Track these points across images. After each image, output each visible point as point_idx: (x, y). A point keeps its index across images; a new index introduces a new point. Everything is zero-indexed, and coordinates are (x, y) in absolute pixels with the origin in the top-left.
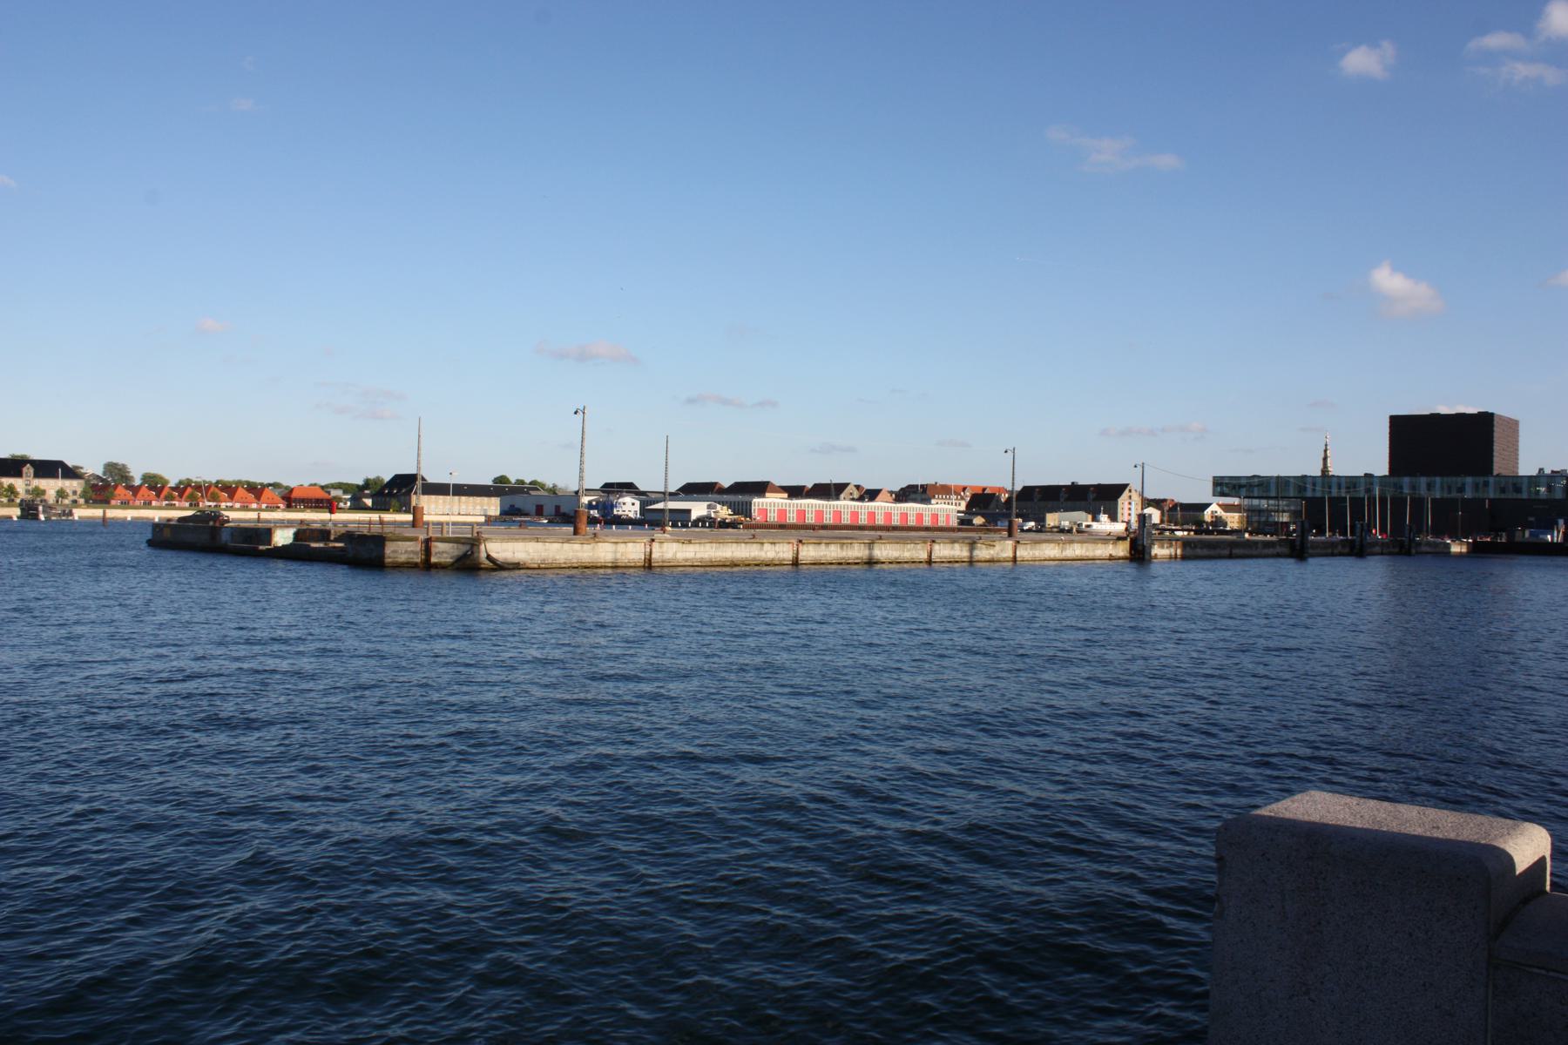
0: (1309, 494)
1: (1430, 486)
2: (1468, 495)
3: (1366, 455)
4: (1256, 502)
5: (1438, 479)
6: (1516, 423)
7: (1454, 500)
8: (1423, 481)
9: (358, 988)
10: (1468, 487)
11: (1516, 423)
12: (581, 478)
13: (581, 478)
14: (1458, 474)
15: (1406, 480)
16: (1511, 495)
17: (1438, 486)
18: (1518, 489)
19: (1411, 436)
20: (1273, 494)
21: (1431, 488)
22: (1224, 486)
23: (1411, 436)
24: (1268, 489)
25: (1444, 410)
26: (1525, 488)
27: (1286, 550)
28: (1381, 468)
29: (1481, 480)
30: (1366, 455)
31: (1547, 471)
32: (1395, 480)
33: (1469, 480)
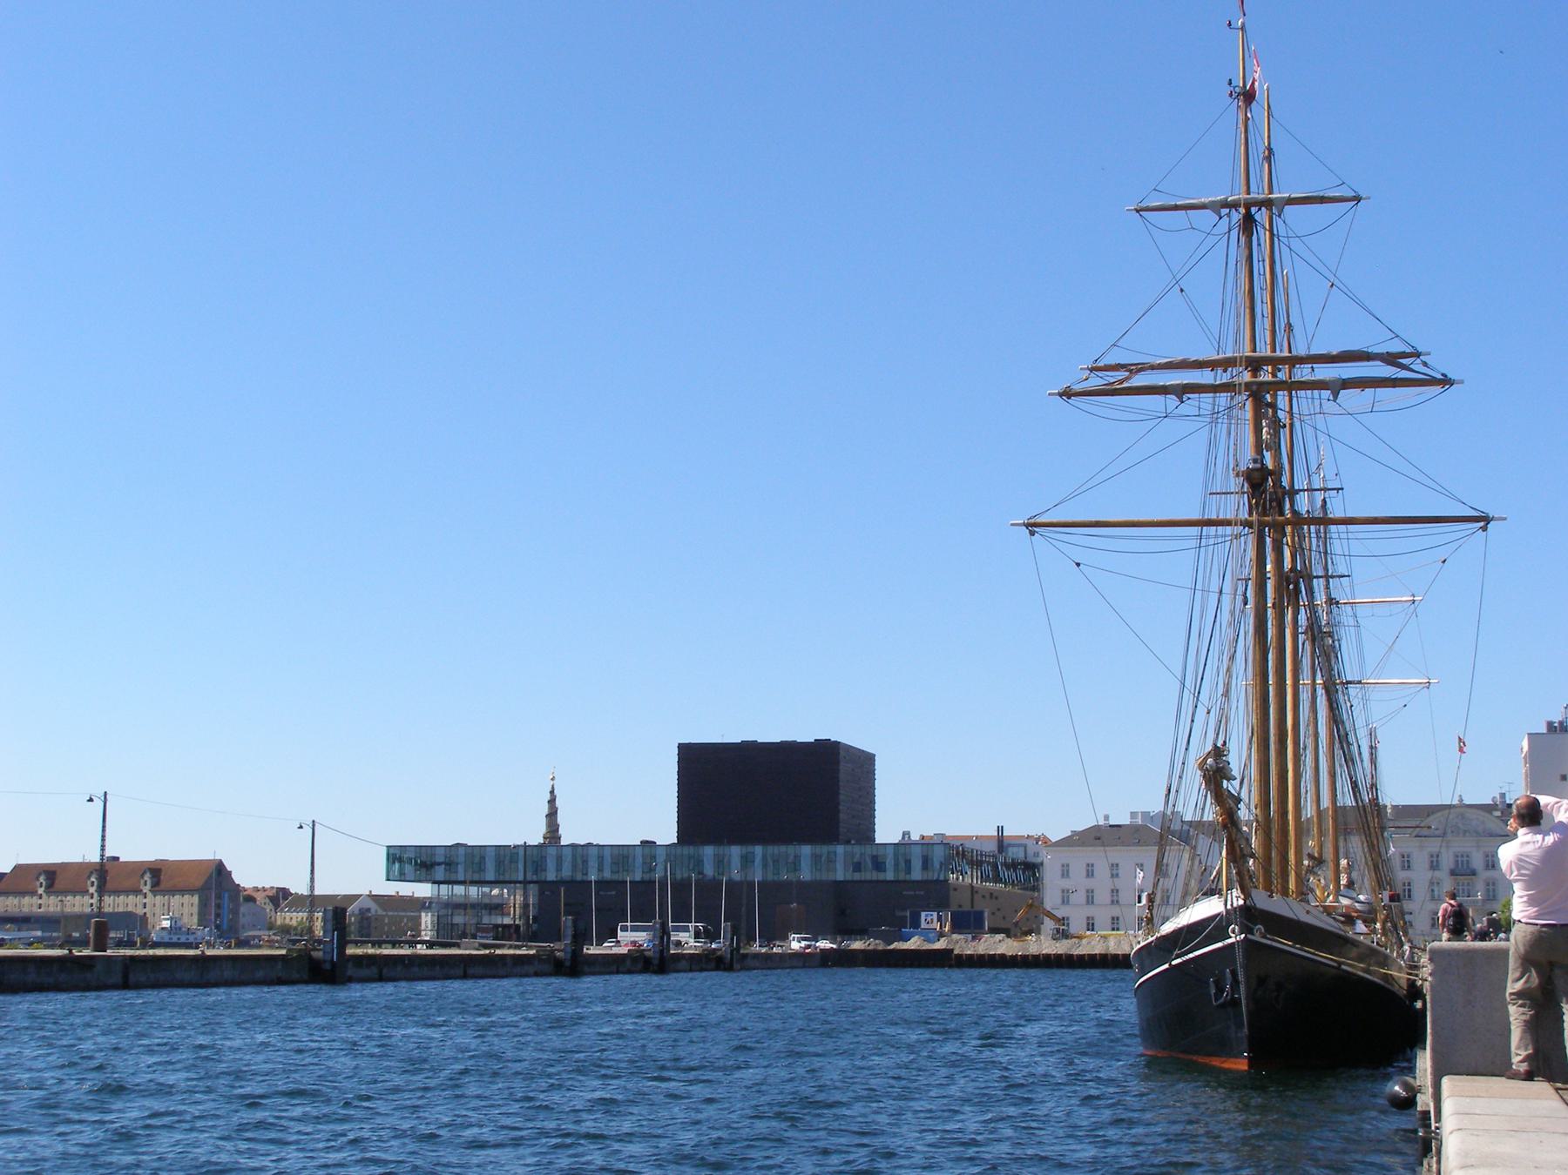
0: (551, 876)
1: (747, 861)
2: (806, 875)
3: (635, 809)
4: (459, 890)
5: (758, 850)
6: (681, 747)
7: (788, 884)
8: (735, 851)
9: (1062, 1166)
10: (806, 862)
11: (681, 747)
12: (103, 848)
13: (103, 848)
14: (788, 841)
15: (709, 851)
16: (870, 875)
17: (840, 866)
18: (879, 865)
19: (720, 784)
20: (490, 876)
21: (743, 864)
22: (410, 861)
23: (720, 784)
24: (481, 866)
25: (762, 738)
26: (890, 863)
27: (548, 968)
28: (665, 831)
29: (824, 849)
30: (635, 809)
31: (915, 837)
32: (688, 850)
33: (806, 850)
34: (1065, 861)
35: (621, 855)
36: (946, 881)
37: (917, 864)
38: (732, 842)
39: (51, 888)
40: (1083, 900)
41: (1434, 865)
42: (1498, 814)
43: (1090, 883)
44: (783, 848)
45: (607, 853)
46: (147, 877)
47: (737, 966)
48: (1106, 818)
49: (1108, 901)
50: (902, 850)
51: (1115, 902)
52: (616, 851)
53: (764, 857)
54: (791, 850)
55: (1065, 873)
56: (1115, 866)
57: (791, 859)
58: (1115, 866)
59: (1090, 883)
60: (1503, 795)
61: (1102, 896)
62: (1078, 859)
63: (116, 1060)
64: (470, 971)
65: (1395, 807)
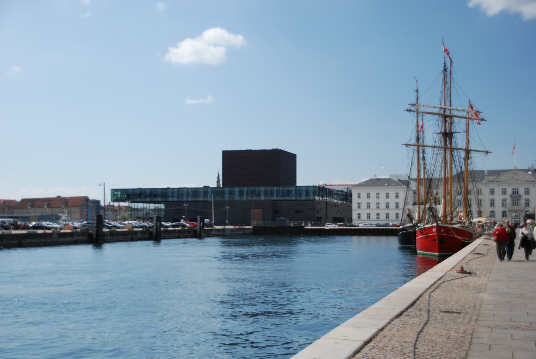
1: (241, 193)
5: (245, 189)
19: (236, 163)
34: (387, 192)
35: (195, 191)
36: (314, 200)
37: (304, 193)
38: (235, 186)
39: (49, 206)
40: (366, 207)
41: (504, 192)
42: (530, 173)
43: (368, 201)
44: (254, 188)
45: (190, 190)
46: (29, 203)
47: (203, 234)
48: (375, 175)
49: (375, 207)
50: (205, 190)
51: (378, 208)
52: (193, 190)
53: (247, 192)
54: (257, 189)
55: (359, 197)
56: (378, 194)
57: (257, 192)
58: (378, 194)
59: (368, 201)
60: (533, 165)
61: (373, 206)
62: (364, 192)
63: (299, 297)
64: (24, 242)
65: (489, 171)
